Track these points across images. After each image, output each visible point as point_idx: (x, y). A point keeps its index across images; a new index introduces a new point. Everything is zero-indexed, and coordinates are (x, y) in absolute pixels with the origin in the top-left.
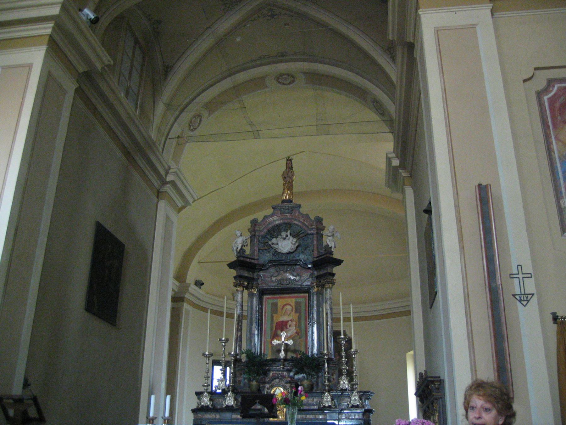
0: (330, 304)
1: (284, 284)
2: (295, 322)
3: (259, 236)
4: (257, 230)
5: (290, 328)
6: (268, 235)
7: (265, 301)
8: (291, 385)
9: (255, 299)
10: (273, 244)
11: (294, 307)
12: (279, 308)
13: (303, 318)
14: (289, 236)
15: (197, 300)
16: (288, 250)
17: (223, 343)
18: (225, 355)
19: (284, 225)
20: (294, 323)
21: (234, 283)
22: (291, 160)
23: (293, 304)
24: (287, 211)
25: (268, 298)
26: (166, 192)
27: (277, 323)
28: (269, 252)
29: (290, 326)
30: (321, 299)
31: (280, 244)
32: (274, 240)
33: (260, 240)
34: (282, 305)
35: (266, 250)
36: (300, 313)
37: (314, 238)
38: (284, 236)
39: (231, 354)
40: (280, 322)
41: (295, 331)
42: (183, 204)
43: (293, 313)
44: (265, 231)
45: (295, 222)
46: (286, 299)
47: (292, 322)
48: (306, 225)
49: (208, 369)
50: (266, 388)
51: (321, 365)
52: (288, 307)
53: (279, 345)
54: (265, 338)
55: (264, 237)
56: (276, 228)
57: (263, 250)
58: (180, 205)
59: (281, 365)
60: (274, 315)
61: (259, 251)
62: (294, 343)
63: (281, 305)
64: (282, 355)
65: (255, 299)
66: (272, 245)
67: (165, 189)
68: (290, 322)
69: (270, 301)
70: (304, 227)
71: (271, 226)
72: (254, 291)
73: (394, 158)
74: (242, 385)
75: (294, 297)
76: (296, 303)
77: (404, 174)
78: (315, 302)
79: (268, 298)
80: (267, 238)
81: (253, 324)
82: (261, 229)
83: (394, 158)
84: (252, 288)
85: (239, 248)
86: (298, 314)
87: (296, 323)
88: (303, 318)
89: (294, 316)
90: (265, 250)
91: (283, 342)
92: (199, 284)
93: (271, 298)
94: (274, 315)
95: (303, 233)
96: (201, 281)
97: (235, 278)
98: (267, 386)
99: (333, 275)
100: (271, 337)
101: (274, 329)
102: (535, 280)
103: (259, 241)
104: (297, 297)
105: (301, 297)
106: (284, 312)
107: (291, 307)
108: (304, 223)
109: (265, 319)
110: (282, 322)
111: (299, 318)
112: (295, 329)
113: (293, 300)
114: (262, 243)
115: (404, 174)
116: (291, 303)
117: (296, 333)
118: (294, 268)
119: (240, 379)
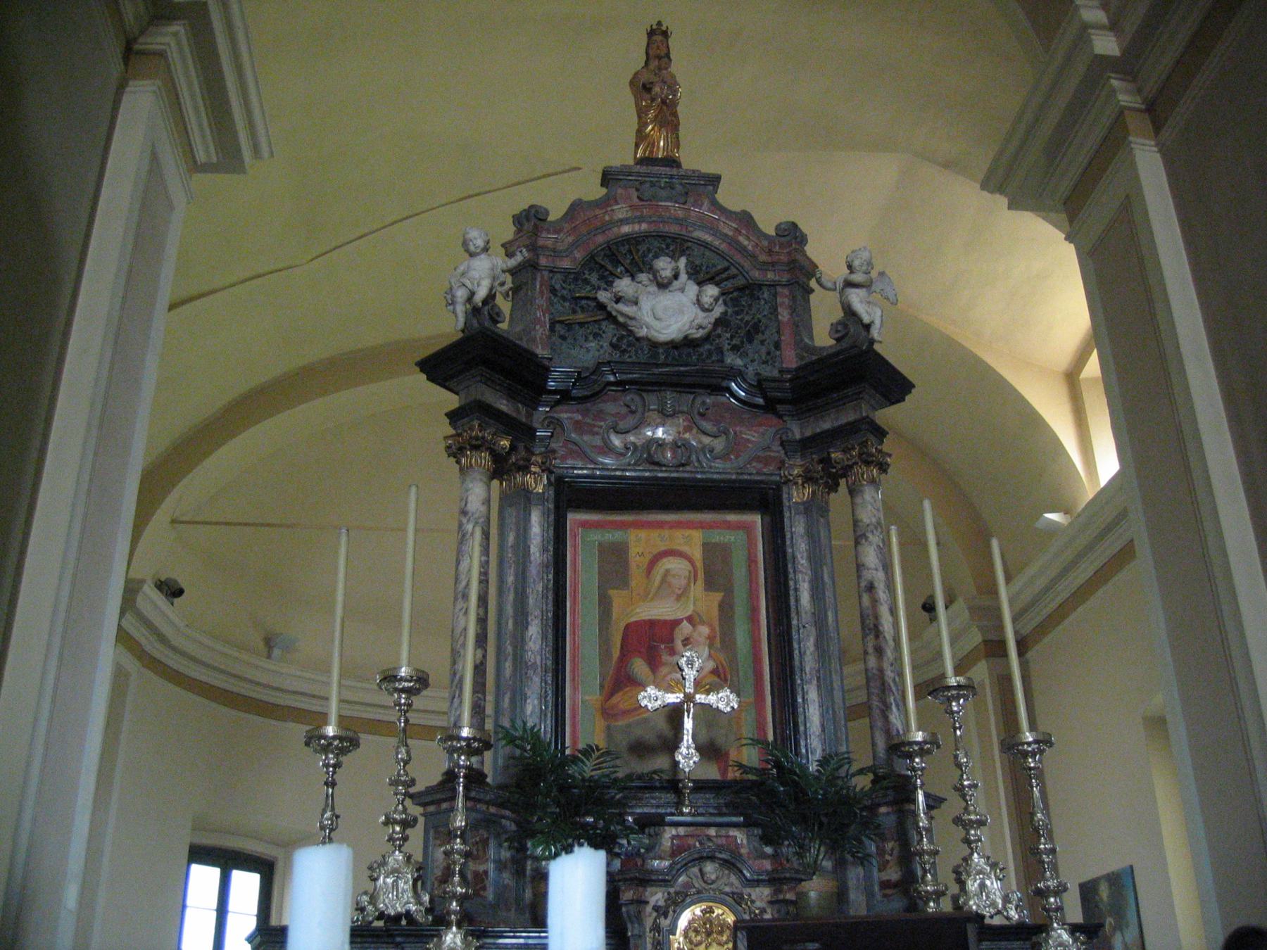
0: (878, 546)
1: (664, 462)
3: (552, 271)
4: (542, 247)
6: (591, 270)
8: (777, 891)
9: (536, 518)
10: (618, 300)
11: (699, 565)
12: (633, 565)
13: (740, 610)
14: (683, 277)
15: (158, 645)
16: (680, 330)
17: (403, 690)
18: (408, 753)
19: (656, 244)
20: (704, 630)
21: (446, 438)
22: (665, 34)
23: (697, 554)
24: (664, 193)
26: (161, 54)
27: (628, 627)
28: (596, 335)
29: (686, 642)
31: (646, 304)
32: (624, 285)
33: (558, 287)
34: (648, 558)
35: (581, 324)
36: (729, 591)
37: (779, 300)
38: (667, 273)
39: (459, 739)
41: (711, 665)
42: (214, 160)
43: (698, 589)
44: (579, 255)
45: (699, 234)
46: (666, 533)
47: (694, 626)
48: (744, 249)
49: (333, 809)
50: (649, 909)
52: (671, 564)
53: (674, 715)
54: (575, 689)
55: (575, 277)
56: (624, 250)
57: (569, 326)
58: (201, 157)
60: (612, 592)
61: (552, 329)
64: (687, 756)
65: (536, 518)
66: (613, 307)
67: (160, 39)
68: (686, 628)
69: (596, 536)
70: (738, 258)
71: (600, 239)
72: (538, 484)
73: (1102, 27)
74: (490, 895)
75: (702, 526)
76: (707, 547)
77: (1124, 99)
79: (584, 524)
80: (587, 282)
81: (527, 623)
82: (560, 247)
83: (1102, 27)
84: (525, 469)
85: (482, 293)
86: (718, 596)
87: (713, 629)
88: (740, 610)
89: (703, 601)
90: (577, 327)
92: (173, 591)
94: (612, 592)
95: (734, 277)
96: (176, 581)
97: (454, 416)
98: (657, 897)
99: (880, 433)
100: (602, 686)
101: (616, 653)
102: (969, 669)
103: (553, 291)
105: (729, 526)
106: (657, 583)
107: (690, 568)
108: (738, 242)
109: (573, 612)
110: (652, 624)
111: (726, 609)
112: (710, 656)
113: (697, 536)
114: (564, 299)
115: (1124, 99)
116: (685, 549)
117: (715, 672)
118: (704, 403)
119: (481, 868)
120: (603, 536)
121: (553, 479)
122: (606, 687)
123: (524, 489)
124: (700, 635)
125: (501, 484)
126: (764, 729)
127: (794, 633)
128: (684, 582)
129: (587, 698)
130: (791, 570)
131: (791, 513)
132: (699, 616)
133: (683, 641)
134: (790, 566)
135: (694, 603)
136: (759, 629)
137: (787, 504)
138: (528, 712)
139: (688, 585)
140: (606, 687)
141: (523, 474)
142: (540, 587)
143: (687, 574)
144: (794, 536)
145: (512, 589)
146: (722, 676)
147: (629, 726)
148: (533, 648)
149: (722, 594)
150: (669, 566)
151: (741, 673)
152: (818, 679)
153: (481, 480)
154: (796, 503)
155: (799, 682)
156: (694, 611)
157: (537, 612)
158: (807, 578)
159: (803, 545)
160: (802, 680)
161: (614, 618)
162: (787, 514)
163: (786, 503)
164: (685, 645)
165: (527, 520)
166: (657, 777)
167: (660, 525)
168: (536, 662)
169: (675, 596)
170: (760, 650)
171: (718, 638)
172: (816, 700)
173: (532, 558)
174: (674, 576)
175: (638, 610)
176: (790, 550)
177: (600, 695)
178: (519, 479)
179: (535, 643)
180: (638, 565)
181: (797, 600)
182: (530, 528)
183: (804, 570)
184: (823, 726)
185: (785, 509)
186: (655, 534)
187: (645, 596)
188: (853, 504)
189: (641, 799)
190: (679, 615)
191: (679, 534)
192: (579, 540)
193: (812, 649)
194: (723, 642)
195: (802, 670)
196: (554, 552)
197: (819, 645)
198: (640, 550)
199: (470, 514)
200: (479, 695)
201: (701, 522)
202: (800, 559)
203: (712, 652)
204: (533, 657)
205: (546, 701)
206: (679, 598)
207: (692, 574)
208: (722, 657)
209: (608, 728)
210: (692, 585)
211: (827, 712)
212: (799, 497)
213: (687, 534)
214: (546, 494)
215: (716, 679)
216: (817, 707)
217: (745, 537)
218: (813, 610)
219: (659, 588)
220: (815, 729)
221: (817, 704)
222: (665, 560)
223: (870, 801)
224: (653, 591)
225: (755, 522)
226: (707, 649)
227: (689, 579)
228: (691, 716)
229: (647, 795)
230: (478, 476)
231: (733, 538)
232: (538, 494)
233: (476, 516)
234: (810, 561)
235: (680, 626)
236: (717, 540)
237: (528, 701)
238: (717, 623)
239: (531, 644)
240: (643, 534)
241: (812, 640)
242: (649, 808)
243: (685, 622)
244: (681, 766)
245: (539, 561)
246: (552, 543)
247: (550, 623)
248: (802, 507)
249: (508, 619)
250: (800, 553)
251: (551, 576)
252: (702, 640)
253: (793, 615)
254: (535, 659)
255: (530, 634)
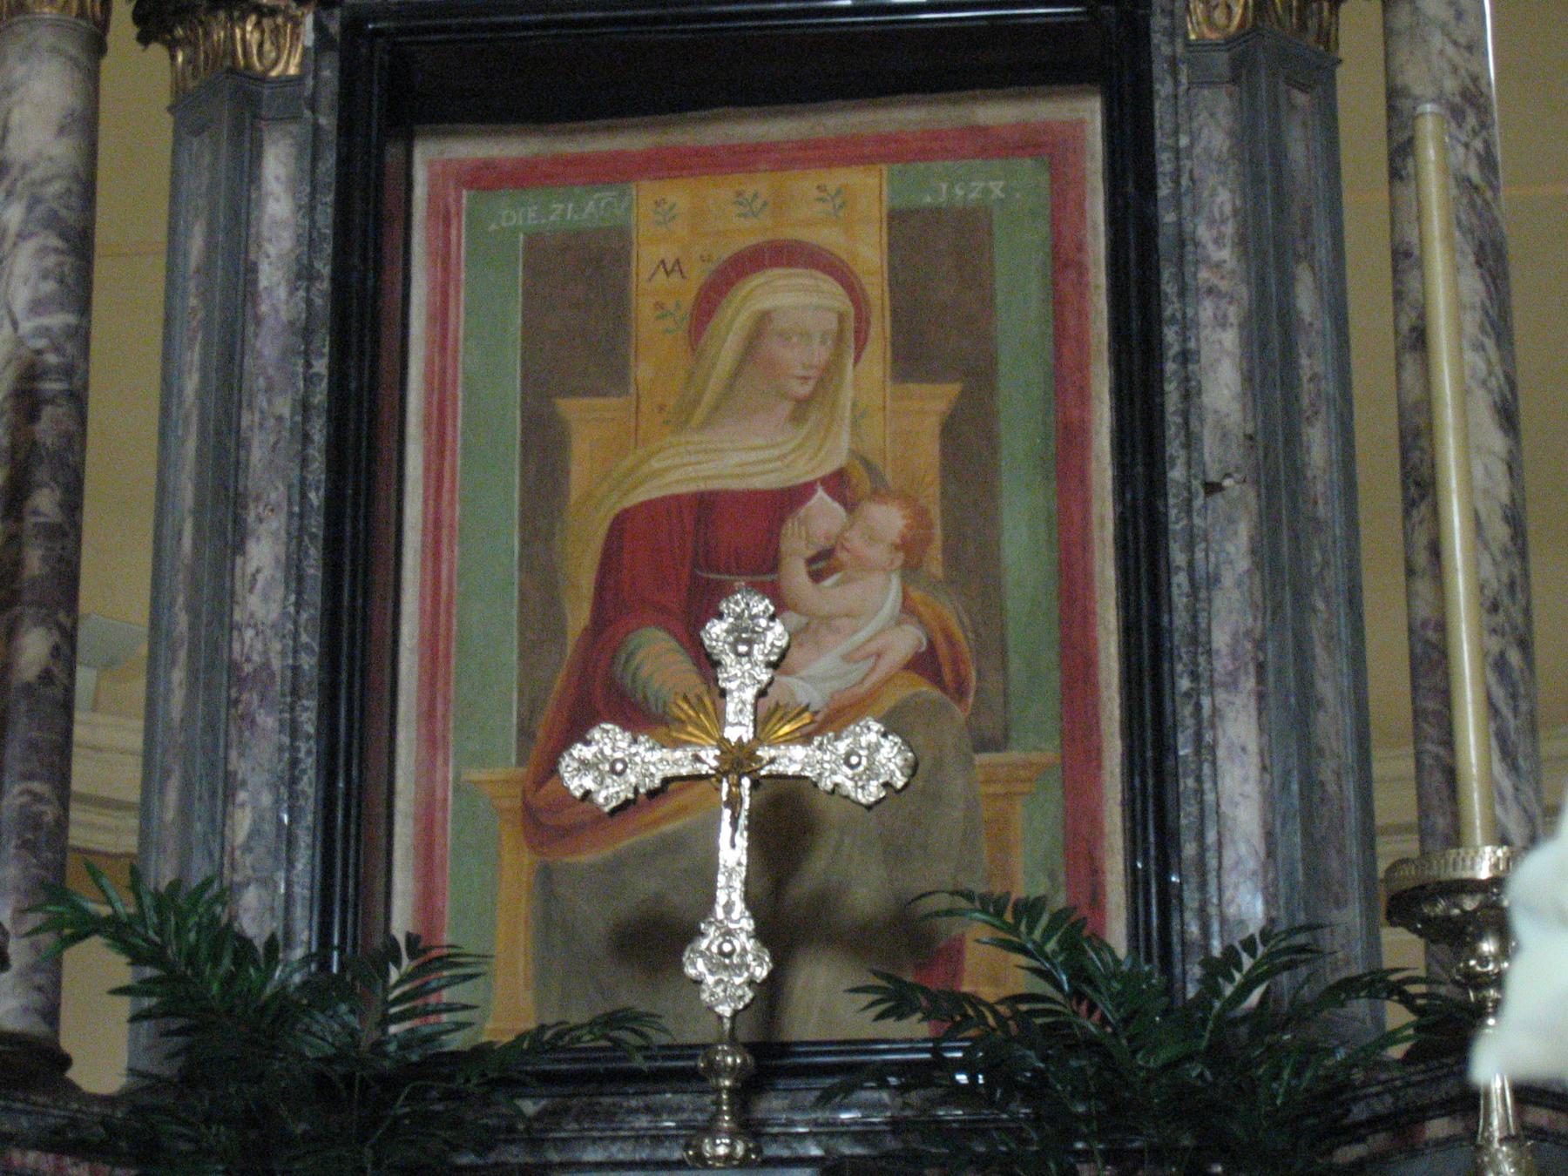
2: (906, 498)
5: (830, 595)
7: (443, 217)
11: (876, 290)
12: (643, 308)
20: (889, 519)
25: (484, 178)
27: (621, 524)
29: (823, 564)
30: (1298, 150)
34: (698, 275)
40: (674, 503)
41: (908, 640)
46: (760, 185)
47: (850, 506)
51: (1354, 1134)
54: (432, 742)
59: (710, 1130)
60: (571, 408)
62: (913, 769)
63: (675, 268)
64: (1141, 12)
68: (824, 512)
78: (1222, 198)
79: (484, 178)
87: (920, 516)
91: (738, 760)
93: (520, 177)
94: (571, 408)
101: (578, 616)
104: (928, 148)
110: (705, 506)
112: (908, 608)
116: (828, 237)
117: (924, 663)
120: (579, 209)
121: (334, 27)
122: (540, 734)
123: (233, 70)
124: (872, 539)
125: (173, 58)
126: (1090, 853)
127: (1173, 513)
128: (820, 353)
129: (475, 775)
130: (1169, 288)
131: (1177, 83)
132: (867, 464)
133: (811, 561)
134: (1166, 274)
135: (855, 424)
136: (1085, 503)
137: (1166, 50)
138: (241, 836)
139: (838, 355)
140: (540, 734)
141: (230, 18)
142: (284, 406)
143: (833, 325)
144: (1187, 164)
145: (194, 419)
146: (948, 675)
147: (615, 866)
148: (260, 614)
149: (953, 389)
150: (767, 303)
151: (1015, 663)
152: (1261, 668)
153: (54, 50)
154: (1204, 45)
155: (1184, 684)
156: (853, 453)
157: (277, 494)
158: (1233, 313)
159: (1224, 196)
160: (1195, 676)
161: (575, 494)
162: (1163, 89)
163: (1161, 46)
164: (817, 577)
165: (247, 171)
166: (634, 1040)
167: (744, 159)
168: (266, 665)
169: (787, 407)
170: (1088, 575)
171: (938, 543)
172: (1253, 747)
173: (264, 308)
174: (783, 336)
175: (656, 464)
176: (1169, 218)
177: (520, 763)
178: (219, 35)
179: (266, 598)
180: (659, 305)
181: (1189, 394)
182: (260, 204)
183: (1224, 285)
184: (1269, 835)
185: (1159, 69)
186: (719, 193)
187: (681, 417)
188: (1388, 33)
189: (610, 1115)
190: (801, 471)
191: (806, 184)
192: (460, 234)
193: (1243, 564)
194: (952, 556)
195: (1198, 640)
196: (333, 280)
197: (1266, 555)
198: (668, 252)
199: (15, 172)
200: (37, 786)
201: (881, 140)
202: (1211, 247)
203: (916, 595)
204: (259, 646)
205: (293, 796)
206: (801, 409)
207: (850, 324)
208: (950, 612)
209: (546, 877)
210: (850, 366)
211: (1285, 786)
212: (1212, 25)
213: (832, 187)
214: (310, 82)
215: (926, 689)
216: (1254, 772)
217: (1044, 178)
218: (1250, 429)
219: (737, 373)
220: (1243, 849)
221: (1253, 761)
222: (757, 280)
223: (1389, 1099)
224: (708, 398)
225: (1080, 124)
226: (895, 583)
227: (840, 338)
228: (743, 822)
229: (633, 1103)
230: (46, 38)
231: (997, 187)
232: (285, 81)
233: (36, 174)
234: (1246, 253)
235: (802, 512)
236: (943, 199)
237: (242, 796)
238: (935, 490)
239: (254, 602)
240: (678, 195)
241: (1244, 530)
242: (629, 1146)
243: (820, 493)
244: (705, 996)
245: (284, 316)
246: (328, 248)
247: (316, 524)
248: (1222, 60)
249: (183, 520)
250: (1211, 223)
251: (321, 366)
252: (879, 553)
253: (1174, 448)
254: (265, 652)
255: (251, 569)
